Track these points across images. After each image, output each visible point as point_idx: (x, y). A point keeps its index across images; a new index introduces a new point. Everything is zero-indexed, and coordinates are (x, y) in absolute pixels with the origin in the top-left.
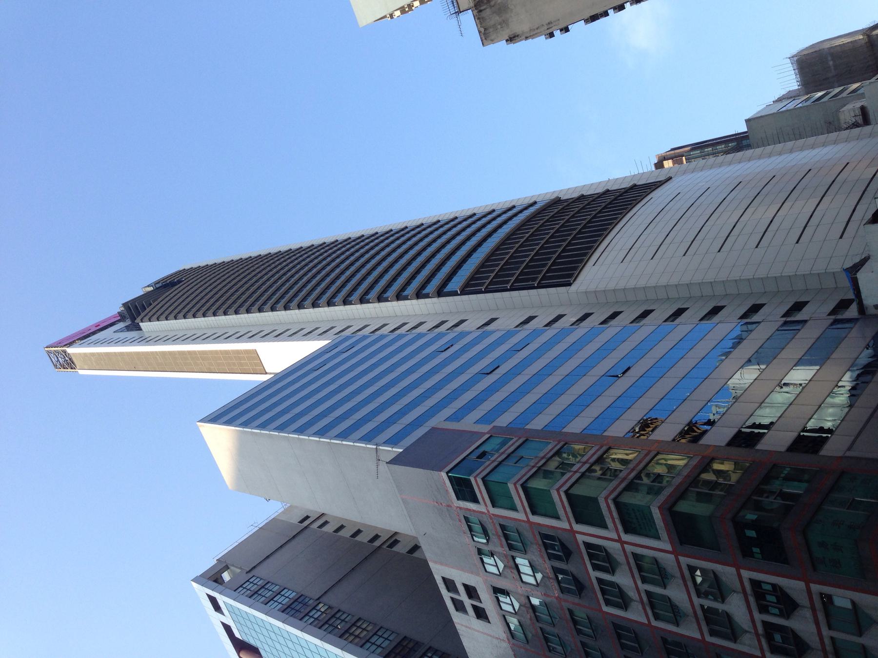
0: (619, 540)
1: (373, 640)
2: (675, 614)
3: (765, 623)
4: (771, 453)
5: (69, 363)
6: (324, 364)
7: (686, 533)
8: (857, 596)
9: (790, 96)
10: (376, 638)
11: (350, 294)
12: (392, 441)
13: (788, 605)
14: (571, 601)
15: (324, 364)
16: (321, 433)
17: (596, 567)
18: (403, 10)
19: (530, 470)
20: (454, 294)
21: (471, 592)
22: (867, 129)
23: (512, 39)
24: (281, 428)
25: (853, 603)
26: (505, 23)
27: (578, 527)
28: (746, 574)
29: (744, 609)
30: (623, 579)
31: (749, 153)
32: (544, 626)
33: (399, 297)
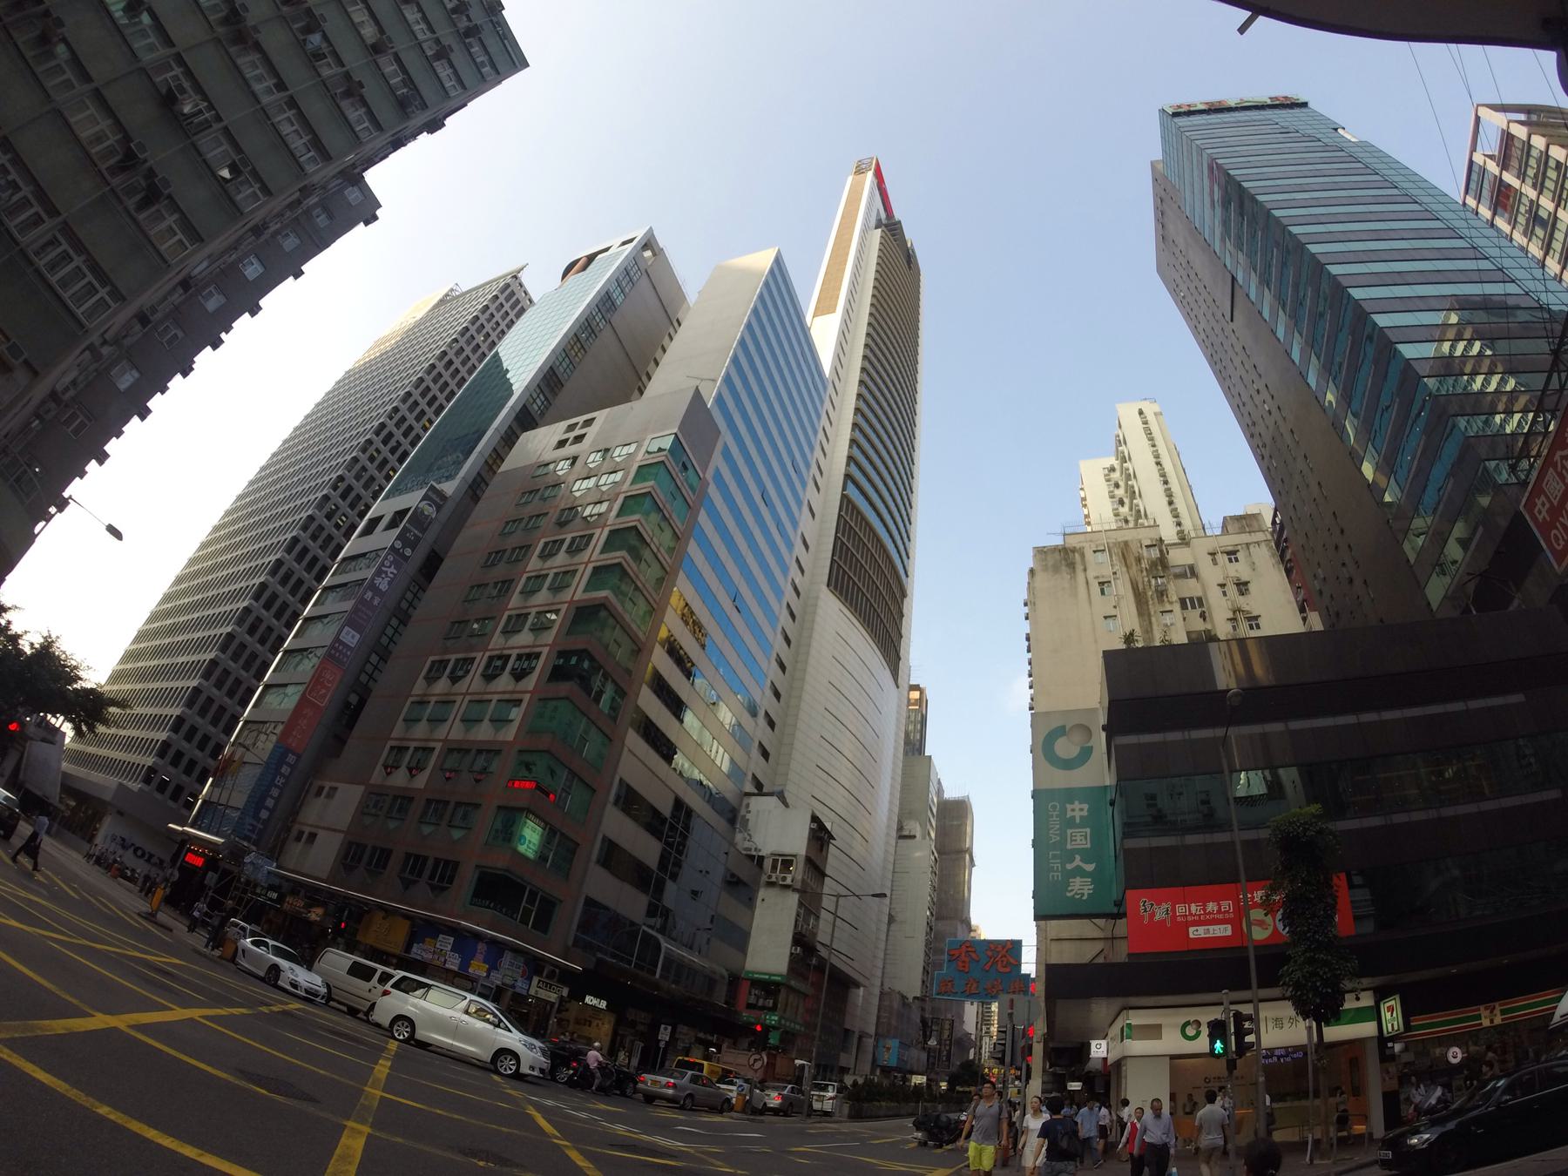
2: (528, 593)
3: (509, 656)
4: (637, 695)
5: (860, 171)
6: (806, 361)
7: (585, 614)
8: (516, 724)
9: (940, 791)
11: (863, 416)
12: (719, 399)
13: (519, 676)
14: (554, 515)
15: (806, 361)
16: (742, 342)
17: (574, 539)
18: (1084, 499)
20: (844, 489)
21: (579, 439)
22: (894, 834)
23: (1032, 571)
24: (755, 311)
26: (1045, 569)
28: (545, 650)
30: (561, 559)
31: (901, 750)
33: (853, 441)
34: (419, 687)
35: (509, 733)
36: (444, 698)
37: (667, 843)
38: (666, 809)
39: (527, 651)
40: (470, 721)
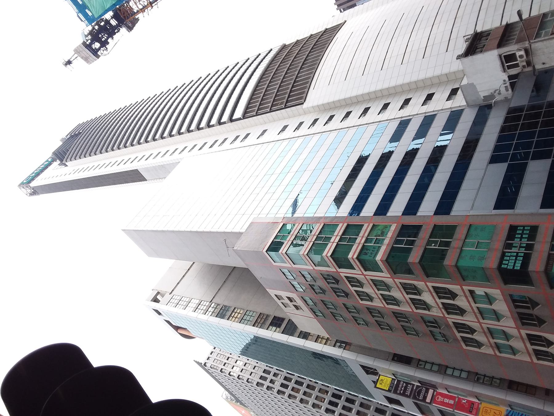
0: (363, 274)
1: (244, 318)
2: (396, 302)
10: (246, 316)
19: (309, 244)
21: (290, 299)
25: (485, 293)
27: (339, 270)
29: (431, 298)
30: (368, 289)
32: (332, 310)
34: (487, 350)
35: (495, 292)
36: (489, 335)
37: (526, 157)
38: (501, 168)
39: (434, 294)
40: (497, 316)
